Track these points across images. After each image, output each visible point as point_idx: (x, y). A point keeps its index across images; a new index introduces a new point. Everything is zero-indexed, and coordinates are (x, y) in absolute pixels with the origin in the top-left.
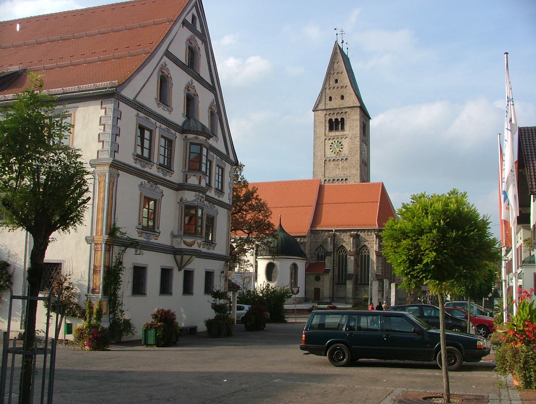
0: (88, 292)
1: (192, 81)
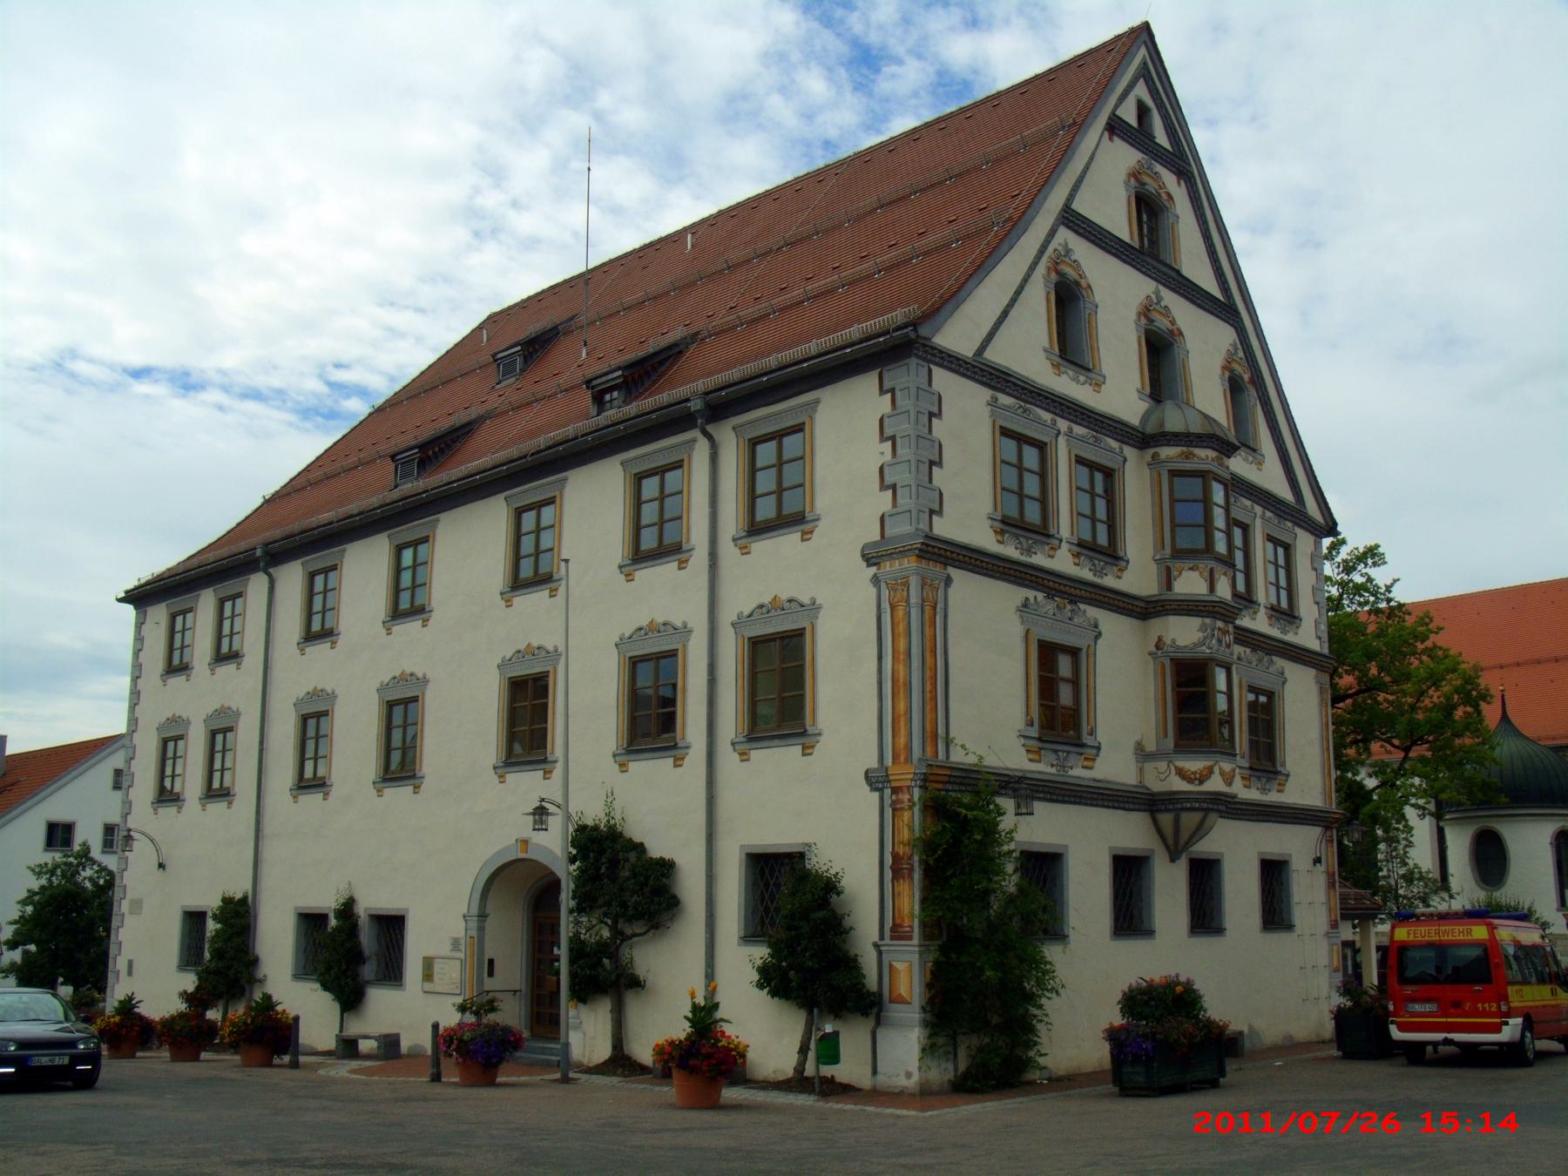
0: (882, 937)
1: (1157, 293)
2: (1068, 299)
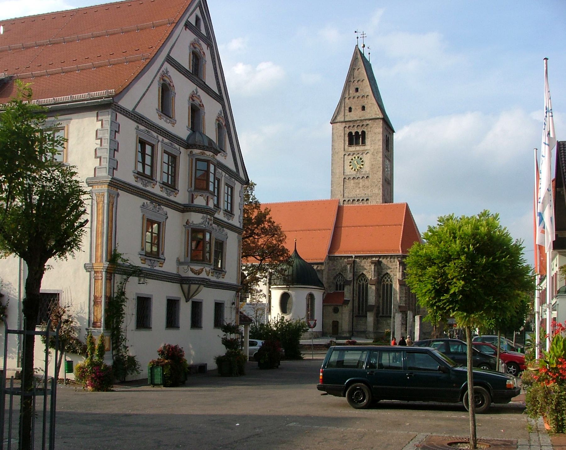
0: (89, 326)
1: (196, 90)
2: (166, 91)
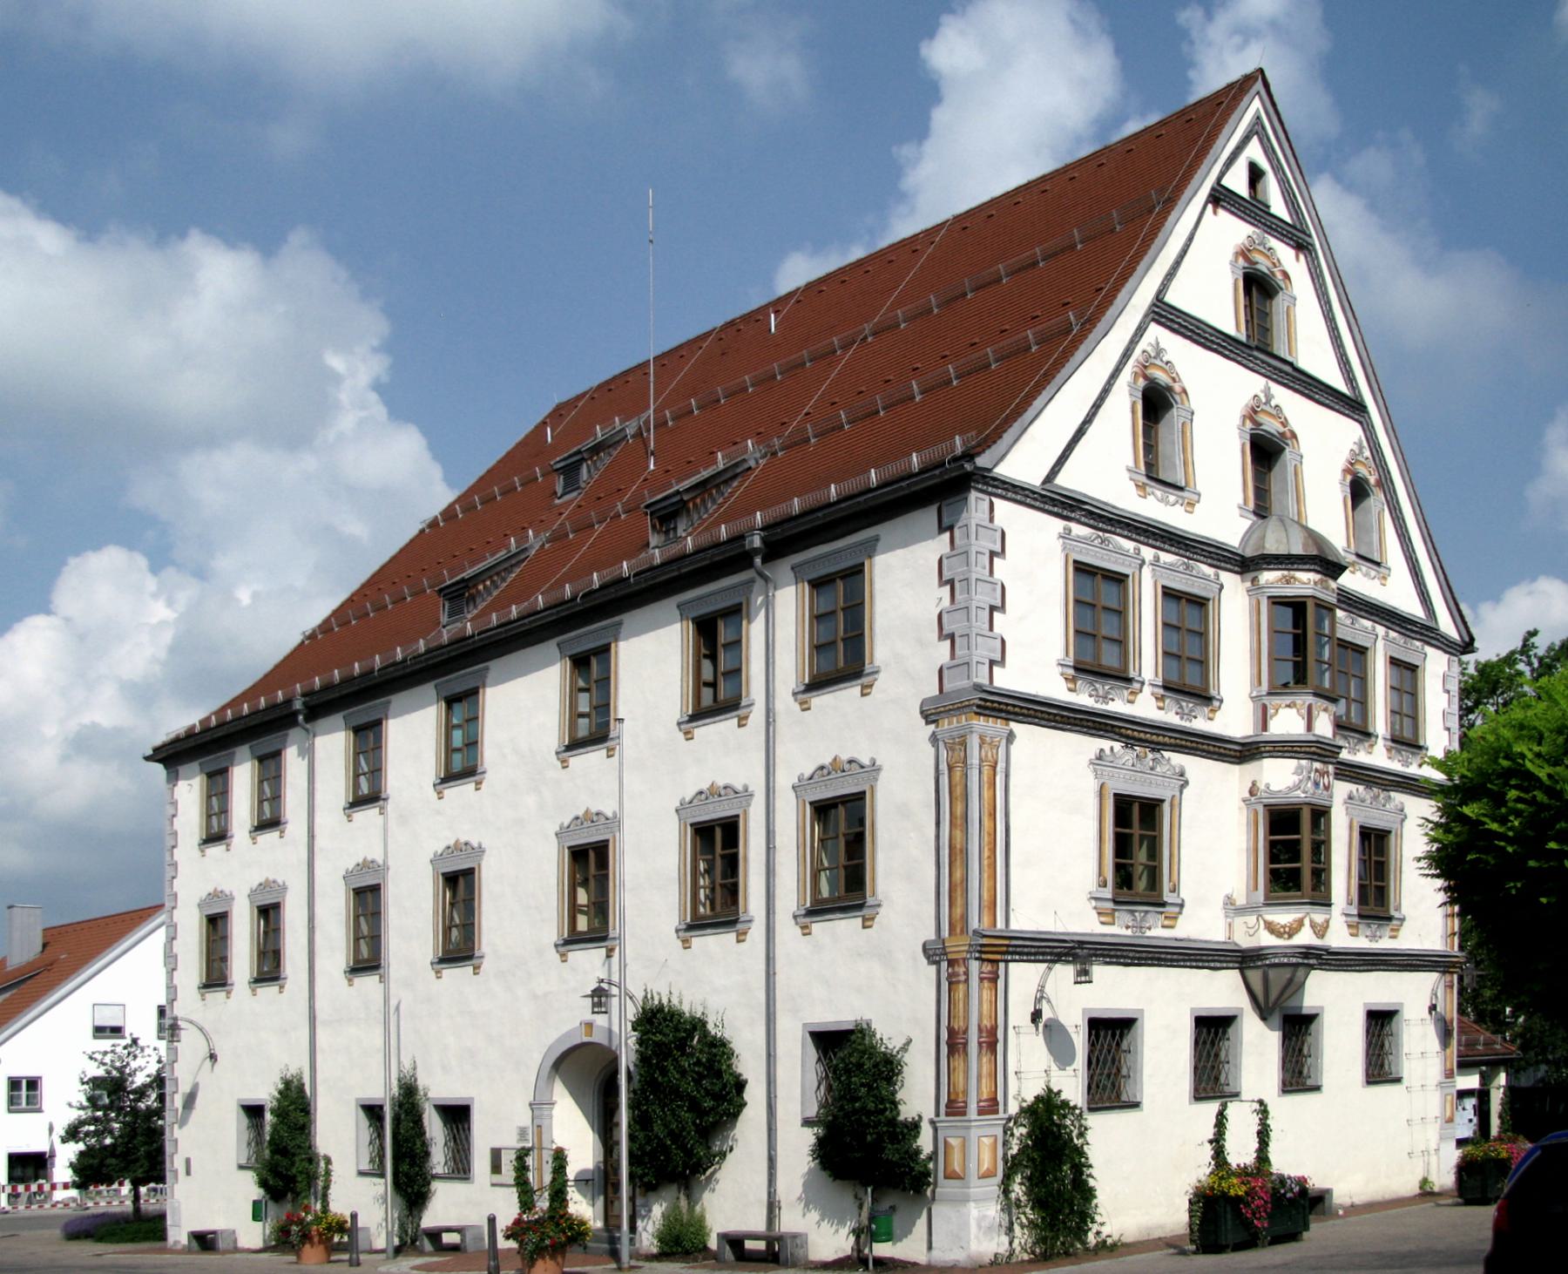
0: (937, 1115)
1: (1267, 392)
